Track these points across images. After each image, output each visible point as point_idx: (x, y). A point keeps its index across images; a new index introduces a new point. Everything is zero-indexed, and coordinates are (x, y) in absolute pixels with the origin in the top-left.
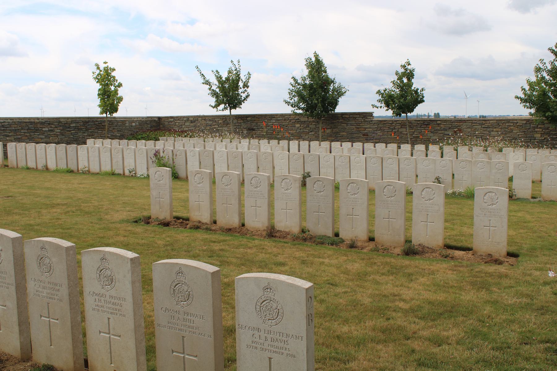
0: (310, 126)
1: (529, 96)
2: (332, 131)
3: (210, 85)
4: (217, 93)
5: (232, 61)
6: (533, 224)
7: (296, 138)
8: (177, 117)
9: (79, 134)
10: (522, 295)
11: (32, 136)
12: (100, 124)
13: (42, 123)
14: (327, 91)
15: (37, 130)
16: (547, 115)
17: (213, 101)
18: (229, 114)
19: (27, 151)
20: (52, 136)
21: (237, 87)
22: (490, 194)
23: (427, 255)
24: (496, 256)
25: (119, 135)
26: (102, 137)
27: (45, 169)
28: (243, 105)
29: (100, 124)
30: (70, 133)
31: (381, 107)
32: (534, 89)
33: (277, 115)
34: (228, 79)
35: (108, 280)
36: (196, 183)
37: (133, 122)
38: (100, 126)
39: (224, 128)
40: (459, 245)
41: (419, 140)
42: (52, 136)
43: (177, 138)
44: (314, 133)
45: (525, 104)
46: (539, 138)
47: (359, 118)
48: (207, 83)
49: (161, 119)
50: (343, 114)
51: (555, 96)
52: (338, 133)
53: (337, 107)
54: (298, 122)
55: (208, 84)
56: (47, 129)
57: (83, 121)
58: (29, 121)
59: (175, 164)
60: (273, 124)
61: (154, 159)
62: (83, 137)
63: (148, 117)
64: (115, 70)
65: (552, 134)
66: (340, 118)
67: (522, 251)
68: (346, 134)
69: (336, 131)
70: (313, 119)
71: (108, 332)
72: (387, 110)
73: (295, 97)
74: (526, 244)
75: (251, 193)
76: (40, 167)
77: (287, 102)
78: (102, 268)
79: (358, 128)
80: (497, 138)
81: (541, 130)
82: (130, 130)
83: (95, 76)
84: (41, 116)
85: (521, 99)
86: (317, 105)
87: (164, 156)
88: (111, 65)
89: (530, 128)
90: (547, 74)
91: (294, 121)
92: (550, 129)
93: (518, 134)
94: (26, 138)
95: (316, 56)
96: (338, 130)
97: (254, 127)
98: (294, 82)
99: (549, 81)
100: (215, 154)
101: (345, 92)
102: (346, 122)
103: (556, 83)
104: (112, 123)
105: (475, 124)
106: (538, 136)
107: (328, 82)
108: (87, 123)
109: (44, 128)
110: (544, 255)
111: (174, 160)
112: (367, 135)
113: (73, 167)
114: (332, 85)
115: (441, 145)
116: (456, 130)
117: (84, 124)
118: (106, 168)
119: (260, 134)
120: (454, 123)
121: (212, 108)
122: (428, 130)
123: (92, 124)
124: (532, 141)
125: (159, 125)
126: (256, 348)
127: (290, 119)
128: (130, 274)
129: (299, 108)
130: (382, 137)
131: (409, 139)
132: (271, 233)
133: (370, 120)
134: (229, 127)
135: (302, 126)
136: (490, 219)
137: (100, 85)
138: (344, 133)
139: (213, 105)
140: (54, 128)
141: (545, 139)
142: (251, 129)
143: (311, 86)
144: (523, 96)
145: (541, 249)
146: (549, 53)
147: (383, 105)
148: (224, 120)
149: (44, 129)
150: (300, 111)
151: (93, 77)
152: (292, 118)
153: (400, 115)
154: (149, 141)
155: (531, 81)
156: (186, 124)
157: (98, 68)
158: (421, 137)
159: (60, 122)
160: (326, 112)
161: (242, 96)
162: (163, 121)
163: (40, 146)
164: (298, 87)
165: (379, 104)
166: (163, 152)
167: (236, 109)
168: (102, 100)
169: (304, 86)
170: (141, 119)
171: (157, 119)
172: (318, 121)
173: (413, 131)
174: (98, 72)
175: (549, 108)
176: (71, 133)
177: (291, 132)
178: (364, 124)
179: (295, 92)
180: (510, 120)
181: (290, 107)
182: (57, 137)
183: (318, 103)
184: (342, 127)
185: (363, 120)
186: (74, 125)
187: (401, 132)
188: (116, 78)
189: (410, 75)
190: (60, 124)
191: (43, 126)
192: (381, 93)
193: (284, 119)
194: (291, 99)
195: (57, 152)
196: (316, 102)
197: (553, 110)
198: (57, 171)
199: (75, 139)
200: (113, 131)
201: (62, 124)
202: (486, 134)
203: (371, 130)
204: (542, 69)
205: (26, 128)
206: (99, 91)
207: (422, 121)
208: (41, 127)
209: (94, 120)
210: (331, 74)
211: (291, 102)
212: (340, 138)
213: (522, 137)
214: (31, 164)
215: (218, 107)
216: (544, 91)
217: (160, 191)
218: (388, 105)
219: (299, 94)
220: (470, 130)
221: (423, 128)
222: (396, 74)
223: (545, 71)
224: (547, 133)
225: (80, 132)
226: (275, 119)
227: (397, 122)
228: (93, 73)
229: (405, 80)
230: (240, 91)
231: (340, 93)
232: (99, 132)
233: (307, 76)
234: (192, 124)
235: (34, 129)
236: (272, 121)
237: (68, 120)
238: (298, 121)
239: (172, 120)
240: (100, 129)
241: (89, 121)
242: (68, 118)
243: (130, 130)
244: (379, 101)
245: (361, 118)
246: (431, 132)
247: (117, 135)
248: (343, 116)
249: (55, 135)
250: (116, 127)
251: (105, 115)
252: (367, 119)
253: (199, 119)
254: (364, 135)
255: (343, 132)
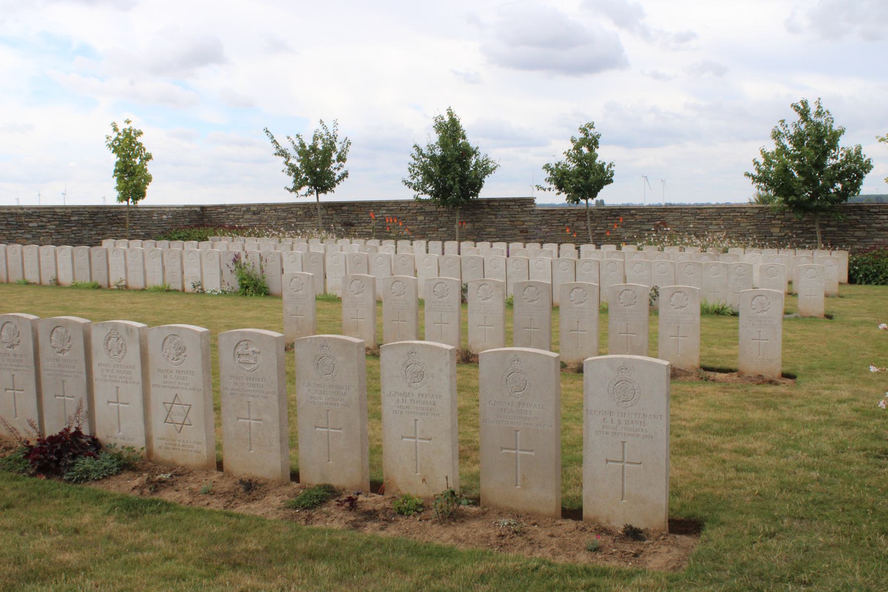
0: (440, 219)
1: (764, 173)
2: (474, 226)
3: (286, 157)
4: (297, 168)
5: (321, 121)
6: (799, 343)
7: (418, 236)
8: (231, 206)
9: (84, 232)
10: (817, 413)
11: (13, 235)
12: (115, 216)
13: (28, 215)
14: (465, 165)
15: (20, 226)
16: (790, 199)
17: (290, 181)
18: (315, 200)
19: (25, 256)
20: (43, 234)
21: (326, 161)
22: (759, 298)
23: (680, 378)
24: (768, 376)
25: (144, 233)
26: (117, 236)
27: (54, 284)
28: (337, 188)
29: (115, 216)
30: (70, 230)
31: (550, 189)
32: (771, 164)
33: (388, 202)
34: (314, 148)
35: (417, 377)
36: (353, 293)
37: (164, 213)
38: (115, 219)
39: (305, 223)
40: (718, 366)
41: (605, 238)
42: (43, 234)
43: (237, 238)
44: (446, 229)
45: (758, 184)
46: (777, 234)
47: (514, 207)
48: (283, 153)
49: (204, 209)
50: (489, 201)
51: (799, 173)
52: (482, 228)
53: (482, 190)
54: (420, 212)
55: (282, 155)
56: (35, 225)
57: (89, 212)
58: (8, 211)
59: (264, 273)
60: (382, 217)
61: (233, 267)
62: (89, 237)
63: (186, 207)
64: (141, 133)
65: (795, 228)
66: (486, 206)
67: (798, 371)
68: (494, 230)
69: (479, 226)
70: (444, 208)
71: (414, 436)
72: (558, 194)
73: (418, 175)
74: (800, 363)
75: (434, 305)
76: (46, 280)
77: (408, 184)
78: (408, 364)
79: (513, 221)
80: (719, 235)
81: (780, 222)
82: (159, 227)
83: (109, 142)
84: (63, 204)
85: (754, 178)
86: (453, 188)
87: (246, 263)
88: (136, 126)
89: (765, 220)
90: (789, 141)
91: (415, 211)
92: (794, 220)
93: (748, 228)
94: (5, 238)
95: (450, 114)
96: (482, 225)
97: (354, 221)
98: (417, 153)
99: (792, 152)
100: (328, 259)
101: (494, 169)
102: (494, 212)
103: (801, 154)
104: (133, 215)
105: (686, 215)
106: (775, 231)
107: (467, 152)
108: (95, 215)
109: (31, 222)
110: (827, 375)
111: (264, 267)
112: (527, 232)
113: (101, 280)
114: (473, 158)
115: (638, 244)
116: (658, 223)
117: (91, 217)
118: (155, 280)
119: (362, 232)
120: (655, 213)
121: (288, 192)
122: (617, 223)
123: (102, 216)
124: (767, 238)
125: (203, 218)
126: (607, 433)
127: (408, 208)
128: (449, 367)
129: (425, 192)
130: (548, 234)
131: (591, 237)
132: (467, 358)
133: (530, 209)
134: (314, 220)
135: (427, 218)
136: (760, 330)
137: (118, 156)
138: (491, 230)
139: (291, 187)
140: (46, 222)
141: (785, 235)
142: (348, 225)
143: (443, 158)
144: (755, 173)
145: (821, 368)
146: (792, 110)
147: (553, 186)
148: (306, 210)
149: (31, 225)
150: (427, 197)
151: (107, 144)
152: (412, 206)
153: (578, 201)
154: (203, 242)
155: (767, 152)
156: (246, 217)
157: (116, 130)
158: (608, 234)
159: (55, 213)
160: (464, 197)
161: (335, 174)
162: (209, 212)
163: (47, 249)
164: (423, 160)
165: (547, 185)
166: (246, 257)
167: (326, 193)
168: (120, 179)
169: (433, 158)
170: (176, 209)
171: (198, 210)
172: (451, 212)
173: (595, 224)
174: (115, 135)
175: (793, 190)
176: (72, 231)
177: (411, 227)
178: (521, 216)
179: (419, 168)
180: (736, 208)
181: (412, 190)
182: (51, 236)
183: (454, 184)
184: (487, 220)
185: (520, 210)
186: (76, 218)
187: (578, 226)
188: (143, 146)
189: (592, 142)
190: (55, 217)
191: (30, 220)
192: (551, 169)
193: (399, 208)
194: (413, 179)
195: (75, 258)
196: (452, 183)
197: (798, 193)
198: (75, 287)
199: (78, 240)
200: (134, 227)
201: (58, 217)
202: (701, 228)
203: (532, 224)
204: (782, 133)
205: (4, 223)
206: (116, 166)
207: (608, 210)
208: (26, 222)
209: (106, 210)
210: (472, 141)
211: (413, 183)
212: (486, 236)
213: (755, 233)
214: (32, 277)
215: (298, 191)
216: (787, 166)
217: (298, 305)
218: (560, 186)
219: (425, 169)
220: (678, 223)
221: (610, 221)
222: (573, 141)
223: (786, 137)
224: (789, 227)
225: (85, 229)
226: (385, 208)
227: (572, 212)
228: (108, 138)
229: (585, 150)
230: (334, 165)
231: (486, 169)
232: (113, 229)
233: (437, 143)
234: (255, 217)
235: (16, 225)
236: (380, 211)
237: (67, 211)
238: (422, 211)
239: (223, 210)
240: (114, 225)
241: (98, 212)
242: (66, 208)
243: (159, 227)
244: (550, 180)
245: (517, 207)
246: (623, 227)
247: (141, 233)
248: (490, 204)
249: (48, 234)
250: (138, 222)
251: (125, 203)
252: (526, 207)
253: (266, 209)
254: (522, 232)
255: (491, 227)
